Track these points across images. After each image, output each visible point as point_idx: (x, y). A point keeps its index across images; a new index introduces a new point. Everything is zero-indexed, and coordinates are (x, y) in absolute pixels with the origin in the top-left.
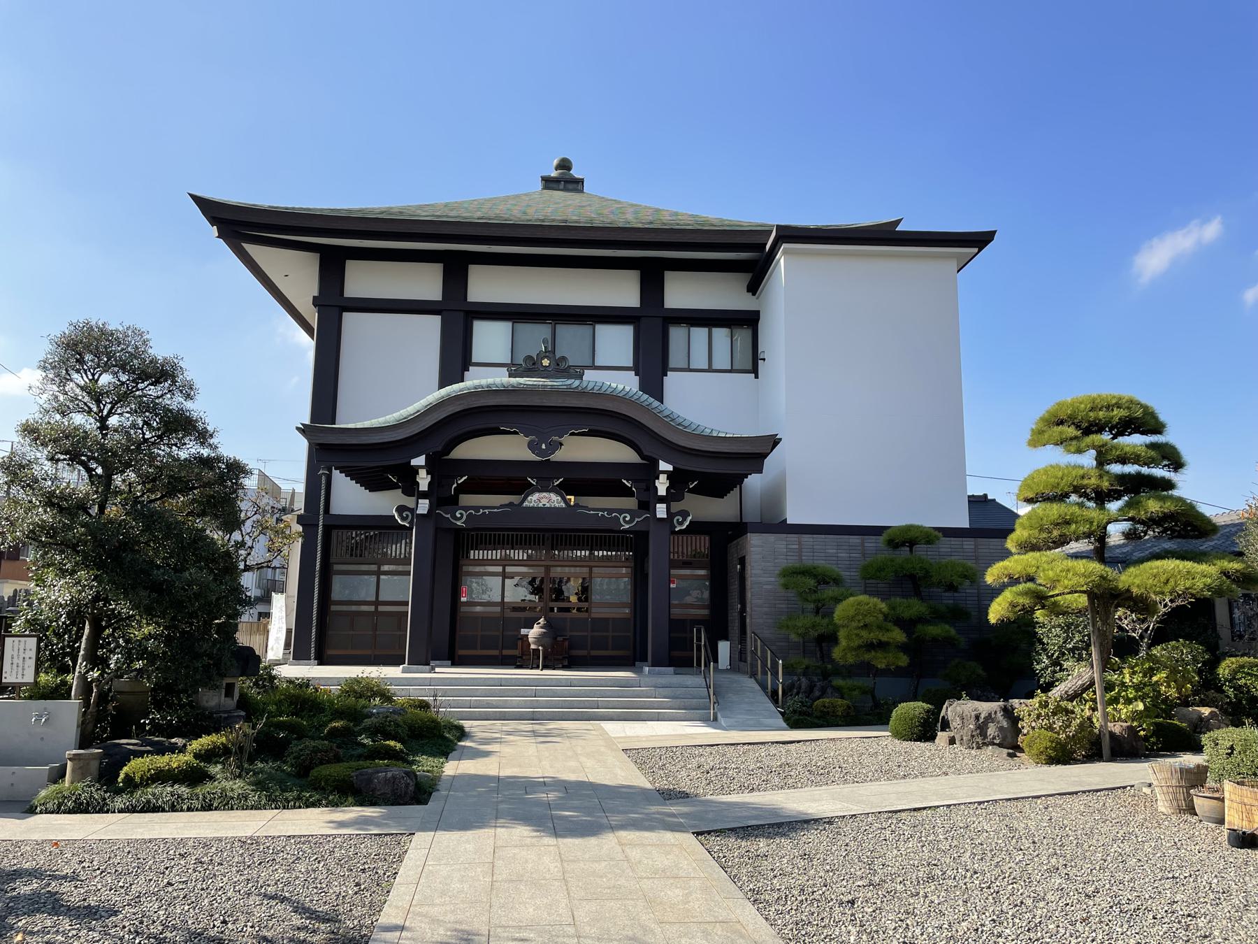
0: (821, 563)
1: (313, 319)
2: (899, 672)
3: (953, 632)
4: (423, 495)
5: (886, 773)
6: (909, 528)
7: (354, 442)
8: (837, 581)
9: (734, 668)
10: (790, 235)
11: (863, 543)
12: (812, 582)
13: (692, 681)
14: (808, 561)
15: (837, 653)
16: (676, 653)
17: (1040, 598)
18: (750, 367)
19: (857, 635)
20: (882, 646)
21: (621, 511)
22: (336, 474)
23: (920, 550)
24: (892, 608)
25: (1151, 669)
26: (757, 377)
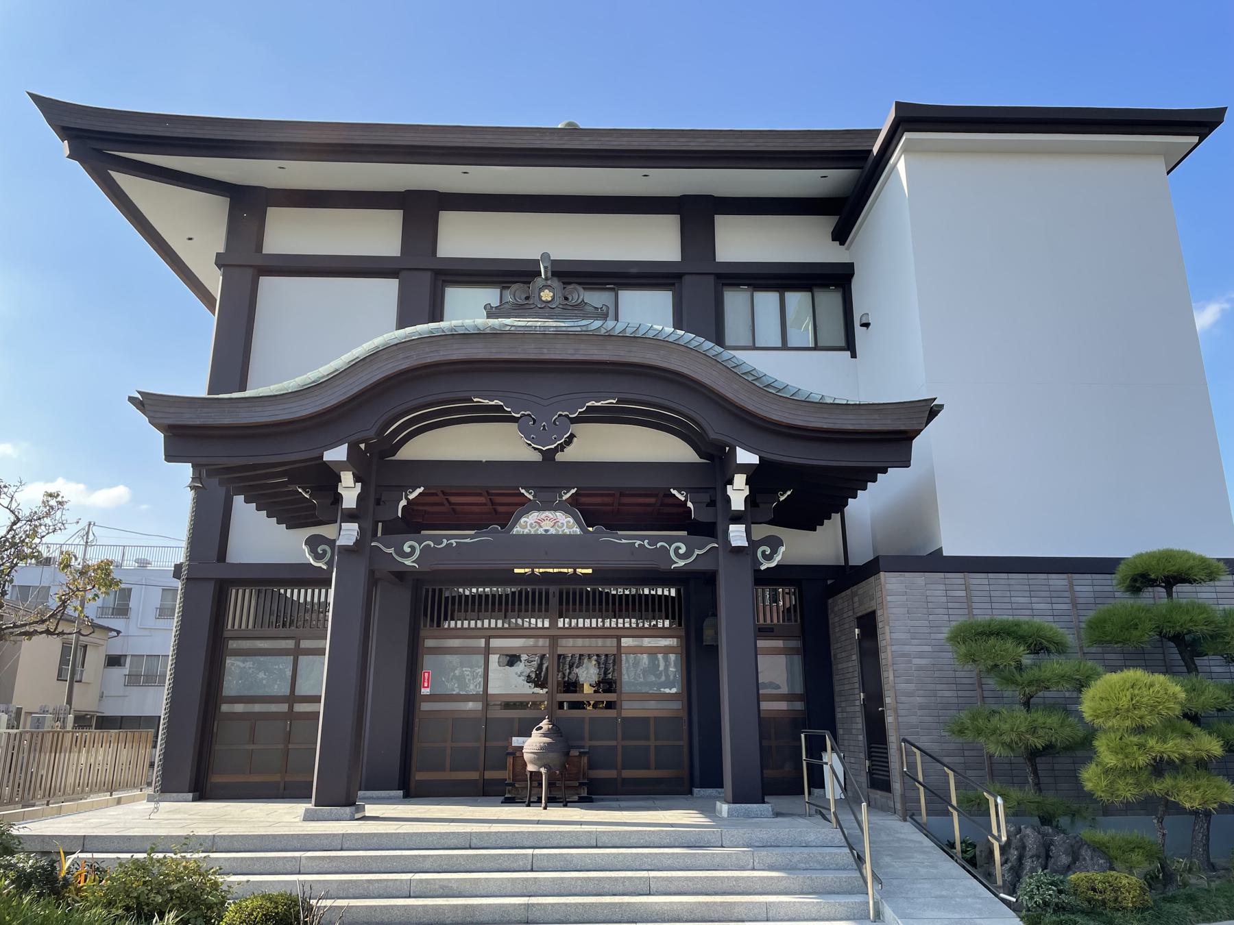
1: (214, 282)
4: (350, 516)
7: (227, 421)
10: (913, 118)
11: (1071, 585)
14: (983, 614)
15: (1090, 777)
18: (843, 343)
19: (1141, 746)
22: (239, 500)
26: (854, 355)
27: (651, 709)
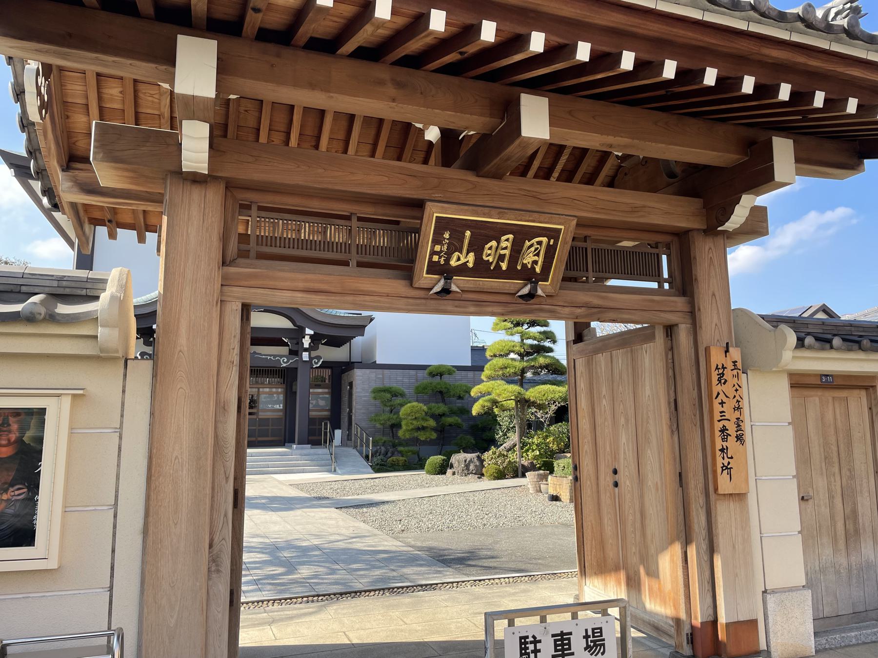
0: (394, 385)
2: (431, 443)
3: (460, 421)
5: (421, 486)
6: (440, 366)
8: (402, 395)
9: (343, 444)
12: (388, 396)
13: (321, 451)
14: (387, 384)
15: (400, 433)
16: (310, 438)
17: (495, 402)
20: (424, 428)
21: (281, 356)
23: (446, 378)
24: (430, 409)
25: (547, 436)
27: (268, 415)
